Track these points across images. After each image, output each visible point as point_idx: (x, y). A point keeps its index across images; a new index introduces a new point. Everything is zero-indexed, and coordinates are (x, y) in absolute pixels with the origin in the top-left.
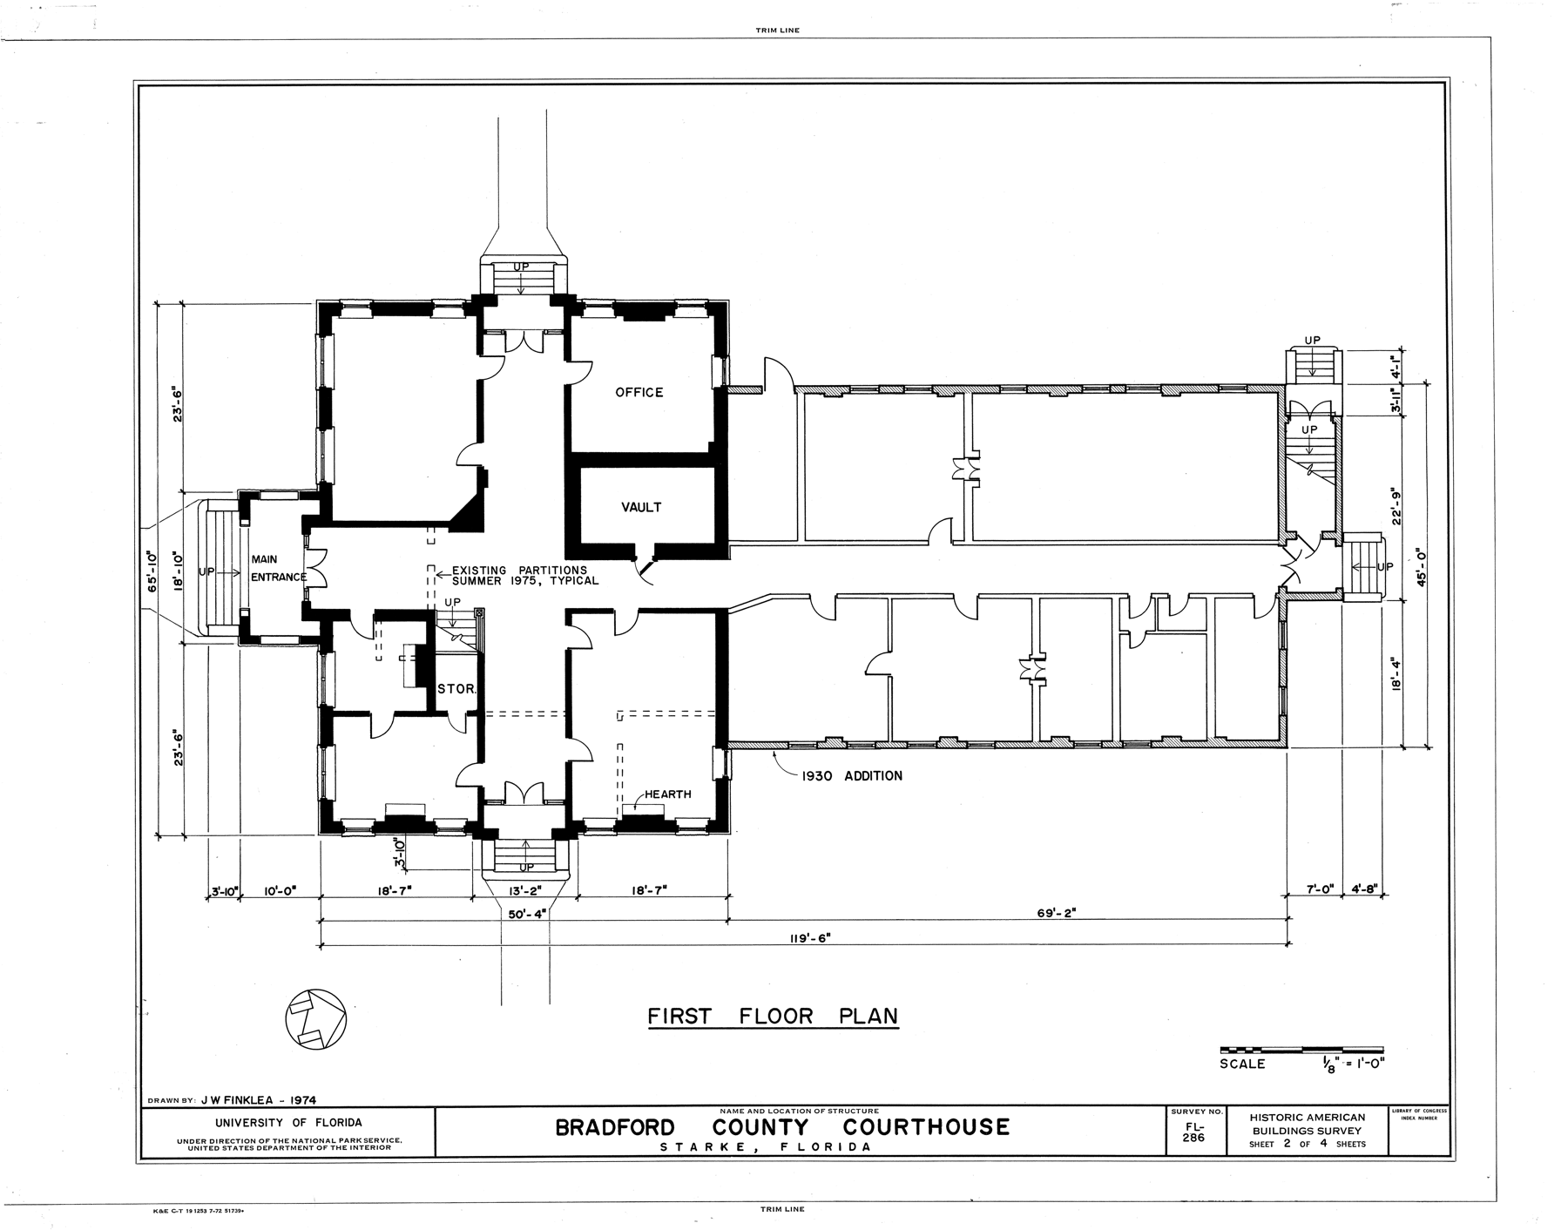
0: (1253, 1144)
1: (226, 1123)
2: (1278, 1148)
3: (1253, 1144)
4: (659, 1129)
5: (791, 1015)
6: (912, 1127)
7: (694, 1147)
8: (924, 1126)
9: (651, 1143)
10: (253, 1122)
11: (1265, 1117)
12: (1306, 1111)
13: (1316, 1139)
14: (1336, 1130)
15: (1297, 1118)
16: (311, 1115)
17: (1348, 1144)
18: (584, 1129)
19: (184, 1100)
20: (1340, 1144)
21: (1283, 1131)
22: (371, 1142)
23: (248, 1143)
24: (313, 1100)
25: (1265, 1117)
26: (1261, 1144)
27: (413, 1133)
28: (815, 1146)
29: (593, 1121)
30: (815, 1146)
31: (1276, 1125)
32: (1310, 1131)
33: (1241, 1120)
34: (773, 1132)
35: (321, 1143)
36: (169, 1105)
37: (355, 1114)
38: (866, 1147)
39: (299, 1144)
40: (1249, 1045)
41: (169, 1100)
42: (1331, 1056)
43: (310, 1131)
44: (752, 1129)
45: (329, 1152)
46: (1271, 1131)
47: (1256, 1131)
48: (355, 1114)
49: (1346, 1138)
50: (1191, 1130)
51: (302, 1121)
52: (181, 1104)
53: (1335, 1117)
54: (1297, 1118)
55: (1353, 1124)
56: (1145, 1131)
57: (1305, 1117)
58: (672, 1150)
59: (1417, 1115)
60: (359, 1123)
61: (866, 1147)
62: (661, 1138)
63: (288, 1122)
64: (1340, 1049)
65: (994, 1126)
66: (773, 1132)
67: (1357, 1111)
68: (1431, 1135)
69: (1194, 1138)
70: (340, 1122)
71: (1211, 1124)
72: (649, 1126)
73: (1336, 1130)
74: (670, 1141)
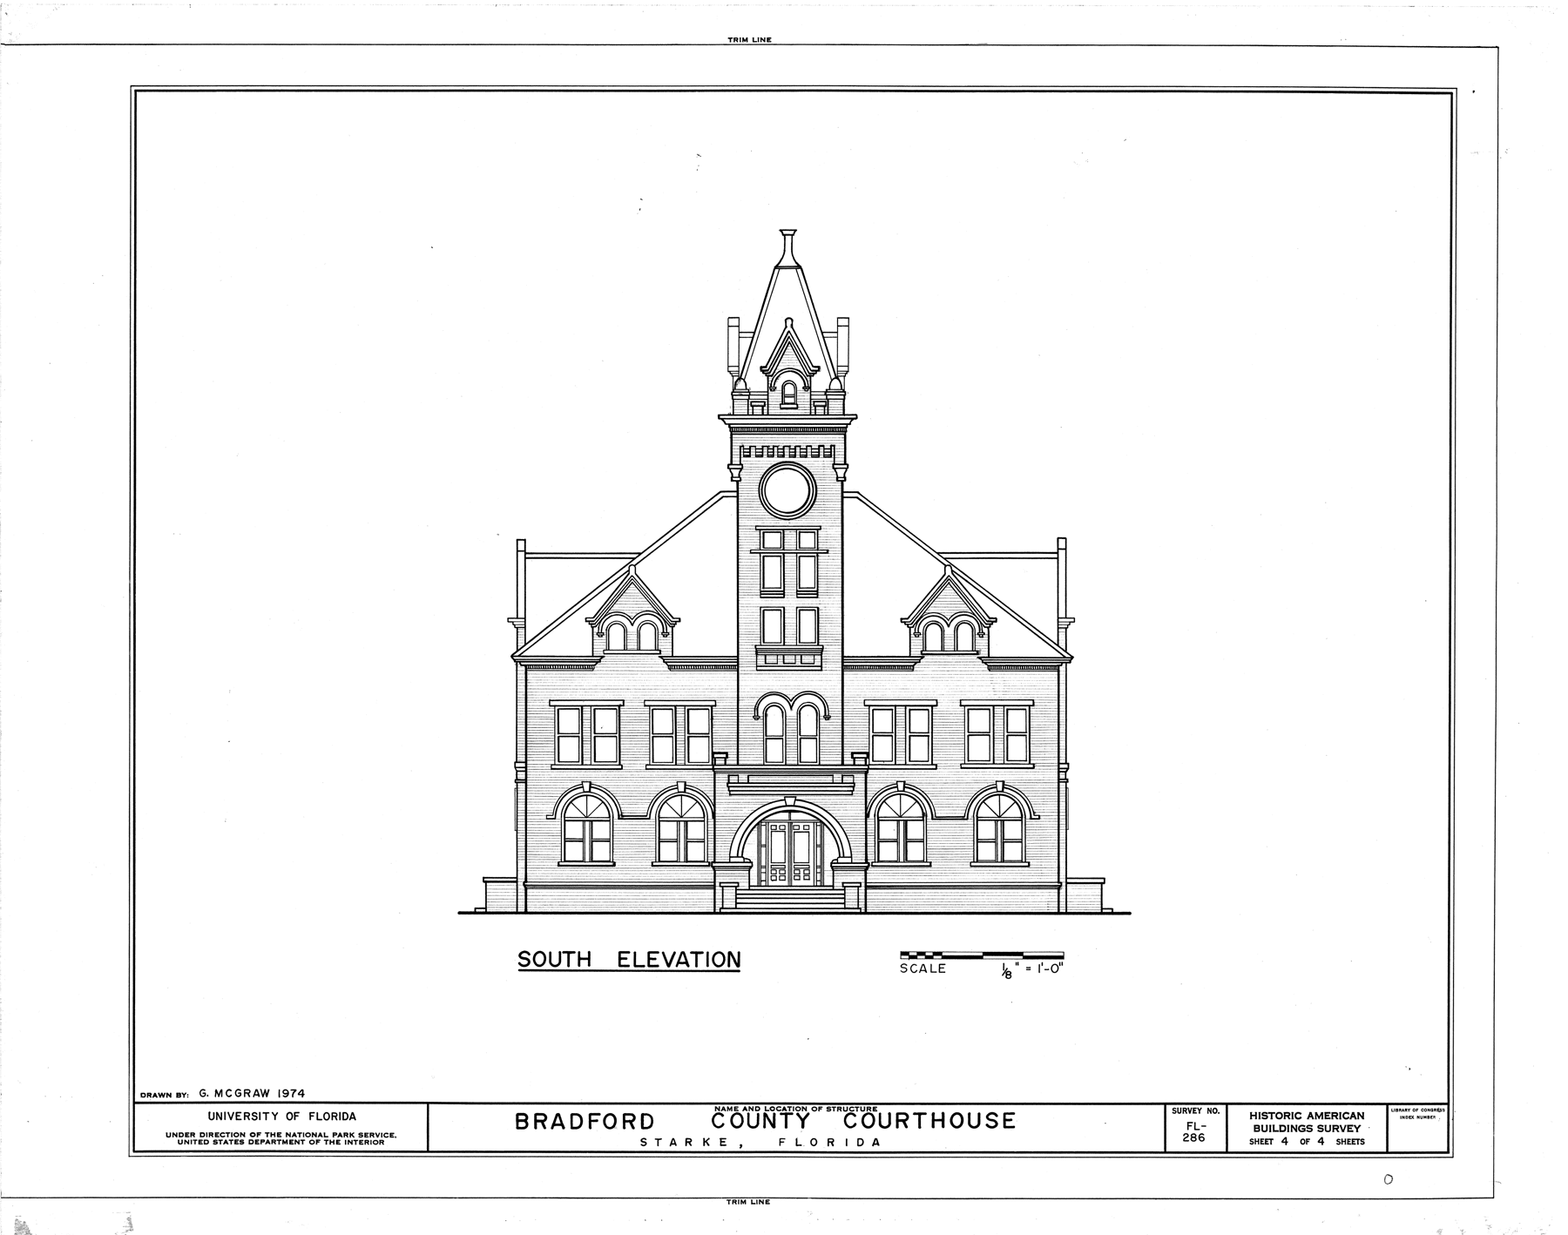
0: (1252, 1142)
1: (218, 1116)
2: (1277, 1146)
3: (1252, 1142)
4: (637, 1123)
5: (719, 959)
6: (913, 1120)
7: (673, 1142)
8: (926, 1120)
9: (628, 1138)
10: (247, 1115)
11: (1265, 1115)
12: (1305, 1110)
13: (1314, 1136)
14: (1335, 1128)
15: (1296, 1116)
16: (304, 1110)
17: (1348, 1142)
18: (549, 1123)
19: (178, 1095)
20: (1339, 1142)
21: (1283, 1129)
22: (365, 1136)
23: (238, 1137)
24: (302, 1093)
25: (1265, 1115)
26: (1261, 1141)
27: (407, 1128)
28: (814, 1142)
29: (558, 1115)
30: (814, 1142)
31: (1277, 1123)
32: (1310, 1129)
33: (1239, 1116)
34: (773, 1126)
35: (315, 1137)
36: (161, 1099)
37: (349, 1109)
38: (876, 1142)
39: (292, 1138)
40: (929, 949)
41: (162, 1095)
42: (1010, 963)
43: (303, 1124)
44: (885, 1123)
45: (322, 1146)
46: (1271, 1128)
47: (1257, 1128)
48: (349, 1109)
49: (1346, 1135)
50: (1191, 1131)
51: (295, 1115)
52: (174, 1098)
53: (1335, 1115)
54: (1296, 1116)
55: (1353, 1122)
56: (1144, 1129)
57: (1305, 1115)
58: (652, 1146)
59: (1415, 1114)
60: (353, 1117)
61: (876, 1142)
62: (639, 1132)
63: (282, 1116)
64: (1020, 954)
65: (1000, 1120)
66: (773, 1126)
67: (1356, 1109)
68: (1430, 1133)
69: (1194, 1137)
70: (334, 1116)
71: (1212, 1126)
72: (628, 1120)
73: (1335, 1128)
74: (650, 1135)
